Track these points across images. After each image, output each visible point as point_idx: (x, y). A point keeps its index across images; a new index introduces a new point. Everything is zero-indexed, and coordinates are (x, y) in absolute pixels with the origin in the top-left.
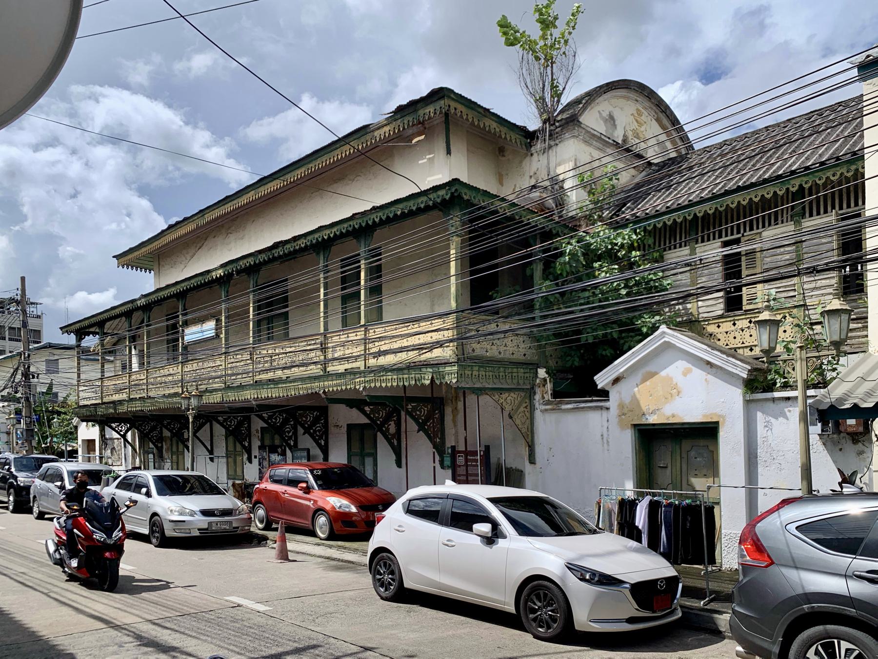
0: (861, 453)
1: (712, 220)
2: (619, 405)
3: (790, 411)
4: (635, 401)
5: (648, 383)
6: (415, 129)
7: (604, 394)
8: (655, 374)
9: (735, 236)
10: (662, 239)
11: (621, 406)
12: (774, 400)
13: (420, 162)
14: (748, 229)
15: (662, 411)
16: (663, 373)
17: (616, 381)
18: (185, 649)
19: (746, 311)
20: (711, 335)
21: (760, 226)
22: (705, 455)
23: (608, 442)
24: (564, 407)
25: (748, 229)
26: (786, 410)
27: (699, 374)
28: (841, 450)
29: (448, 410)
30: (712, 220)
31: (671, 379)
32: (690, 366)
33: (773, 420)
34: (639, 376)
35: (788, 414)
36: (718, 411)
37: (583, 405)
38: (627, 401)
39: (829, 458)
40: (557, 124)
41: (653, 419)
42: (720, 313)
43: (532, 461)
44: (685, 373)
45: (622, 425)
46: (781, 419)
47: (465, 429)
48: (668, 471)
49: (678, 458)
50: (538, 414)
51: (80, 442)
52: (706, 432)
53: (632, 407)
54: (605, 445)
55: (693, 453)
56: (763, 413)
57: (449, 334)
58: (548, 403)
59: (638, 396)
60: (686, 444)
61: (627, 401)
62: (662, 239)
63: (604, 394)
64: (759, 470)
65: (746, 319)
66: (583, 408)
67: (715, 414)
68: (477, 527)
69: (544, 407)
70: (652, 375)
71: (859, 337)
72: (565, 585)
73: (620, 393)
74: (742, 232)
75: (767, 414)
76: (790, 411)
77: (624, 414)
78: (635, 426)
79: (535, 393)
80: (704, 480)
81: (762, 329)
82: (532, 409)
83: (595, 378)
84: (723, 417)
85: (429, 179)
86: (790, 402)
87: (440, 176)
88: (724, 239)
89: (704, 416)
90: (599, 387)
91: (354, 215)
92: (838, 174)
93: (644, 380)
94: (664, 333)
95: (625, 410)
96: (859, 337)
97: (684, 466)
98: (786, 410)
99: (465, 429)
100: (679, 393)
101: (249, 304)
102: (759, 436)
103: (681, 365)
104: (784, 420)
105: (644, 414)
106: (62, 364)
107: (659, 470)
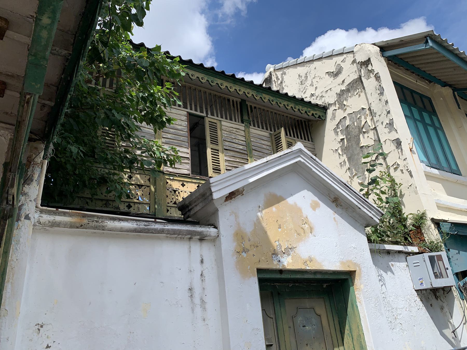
3: (392, 265)
5: (274, 209)
11: (239, 236)
15: (295, 250)
16: (291, 200)
18: (426, 68)
20: (175, 191)
23: (203, 301)
24: (110, 224)
26: (390, 263)
38: (248, 229)
41: (288, 263)
42: (186, 172)
51: (449, 272)
53: (253, 241)
54: (198, 309)
55: (299, 320)
61: (248, 229)
65: (195, 183)
67: (355, 264)
73: (237, 217)
77: (245, 250)
78: (260, 271)
95: (247, 245)
98: (390, 263)
99: (180, 169)
104: (392, 275)
105: (275, 254)
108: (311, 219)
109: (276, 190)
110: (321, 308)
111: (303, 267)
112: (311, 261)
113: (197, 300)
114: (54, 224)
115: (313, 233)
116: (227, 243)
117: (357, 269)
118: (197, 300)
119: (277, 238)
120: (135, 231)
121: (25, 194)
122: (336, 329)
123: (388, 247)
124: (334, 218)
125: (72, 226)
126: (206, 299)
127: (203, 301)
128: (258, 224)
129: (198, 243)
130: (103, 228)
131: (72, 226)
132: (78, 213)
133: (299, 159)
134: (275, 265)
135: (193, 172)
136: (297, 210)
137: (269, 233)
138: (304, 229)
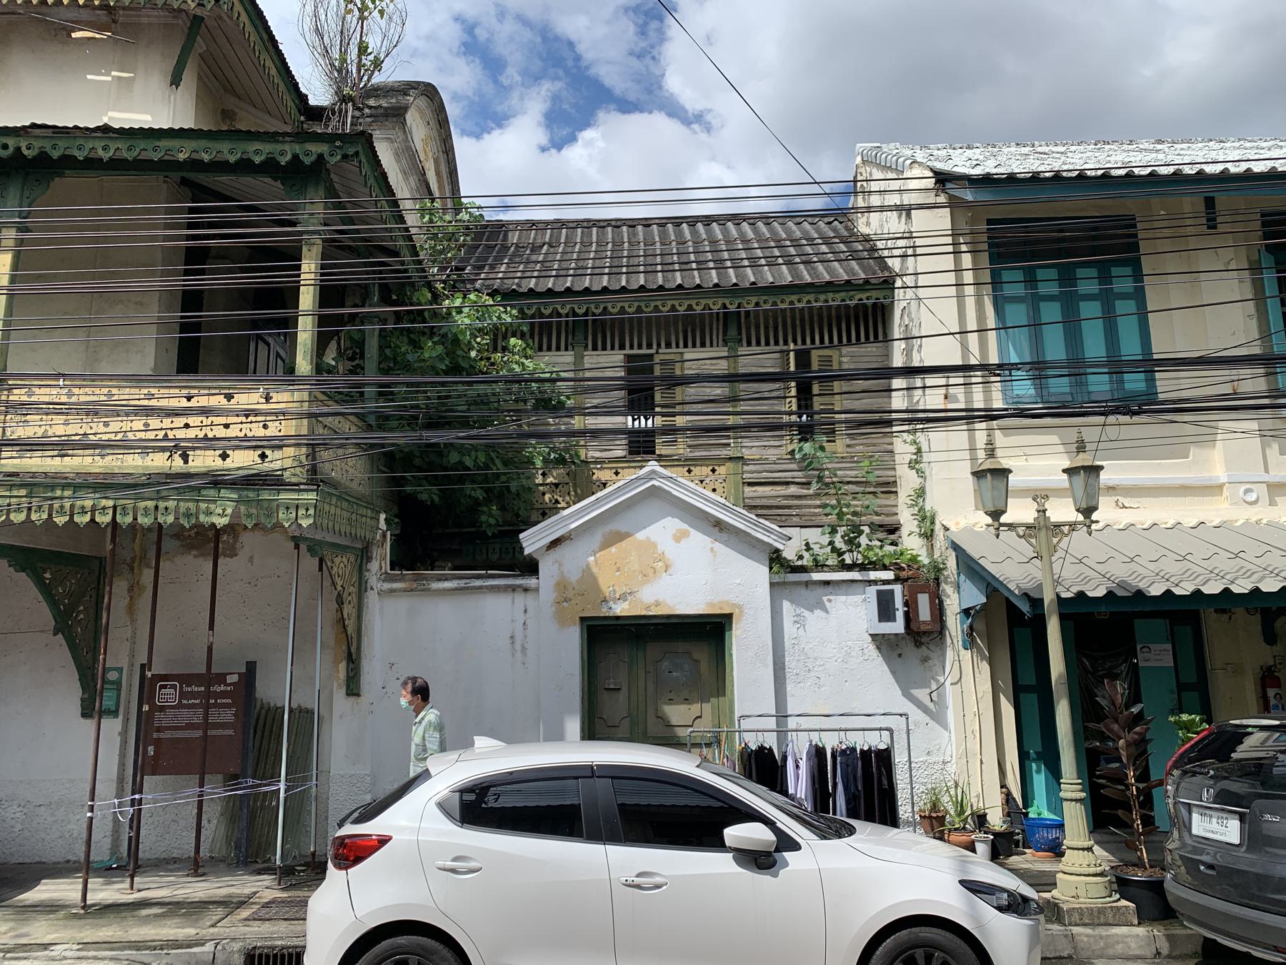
0: (925, 660)
1: (707, 322)
2: (558, 584)
4: (589, 578)
5: (613, 549)
6: (85, 15)
7: (531, 567)
8: (627, 535)
9: (644, 351)
10: (808, 332)
11: (562, 586)
12: (808, 584)
13: (89, 77)
14: (663, 345)
15: (638, 595)
16: (641, 535)
17: (555, 543)
19: (660, 456)
21: (681, 344)
22: (686, 667)
23: (523, 648)
25: (663, 345)
26: (825, 599)
27: (699, 541)
28: (900, 655)
29: (120, 587)
30: (707, 322)
31: (654, 545)
32: (685, 526)
33: (806, 613)
34: (597, 538)
35: (827, 604)
36: (732, 598)
37: (478, 583)
39: (886, 667)
40: (367, 111)
41: (621, 609)
42: (620, 453)
43: (353, 688)
44: (679, 537)
45: (561, 619)
46: (818, 612)
47: (211, 627)
48: (622, 696)
49: (642, 673)
50: (372, 599)
52: (710, 631)
54: (519, 654)
55: (665, 664)
56: (792, 602)
57: (288, 428)
58: (388, 578)
59: (595, 570)
60: (654, 650)
62: (808, 332)
63: (531, 567)
64: (789, 689)
65: (683, 466)
66: (481, 587)
67: (727, 603)
68: (733, 833)
69: (387, 586)
70: (620, 537)
71: (810, 507)
72: (980, 926)
73: (560, 565)
74: (655, 346)
75: (798, 604)
76: (830, 601)
78: (582, 619)
79: (369, 559)
80: (683, 708)
81: (995, 482)
82: (362, 587)
83: (521, 536)
84: (740, 607)
85: (110, 114)
86: (830, 589)
87: (148, 118)
88: (628, 351)
89: (710, 605)
90: (526, 552)
91: (34, 126)
92: (805, 300)
93: (606, 544)
94: (654, 472)
95: (570, 594)
96: (810, 507)
97: (651, 686)
98: (825, 599)
99: (211, 627)
100: (667, 568)
101: (292, 255)
102: (786, 637)
103: (671, 524)
105: (605, 601)
106: (1041, 274)
107: (606, 695)
108: (668, 555)
109: (618, 525)
110: (702, 653)
113: (518, 646)
114: (392, 591)
115: (670, 571)
117: (736, 612)
118: (518, 646)
119: (607, 582)
120: (456, 589)
121: (368, 570)
124: (712, 549)
125: (405, 590)
126: (527, 646)
127: (523, 648)
129: (523, 594)
130: (429, 590)
131: (405, 590)
132: (315, 638)
133: (654, 482)
134: (604, 612)
135: (631, 453)
138: (657, 565)
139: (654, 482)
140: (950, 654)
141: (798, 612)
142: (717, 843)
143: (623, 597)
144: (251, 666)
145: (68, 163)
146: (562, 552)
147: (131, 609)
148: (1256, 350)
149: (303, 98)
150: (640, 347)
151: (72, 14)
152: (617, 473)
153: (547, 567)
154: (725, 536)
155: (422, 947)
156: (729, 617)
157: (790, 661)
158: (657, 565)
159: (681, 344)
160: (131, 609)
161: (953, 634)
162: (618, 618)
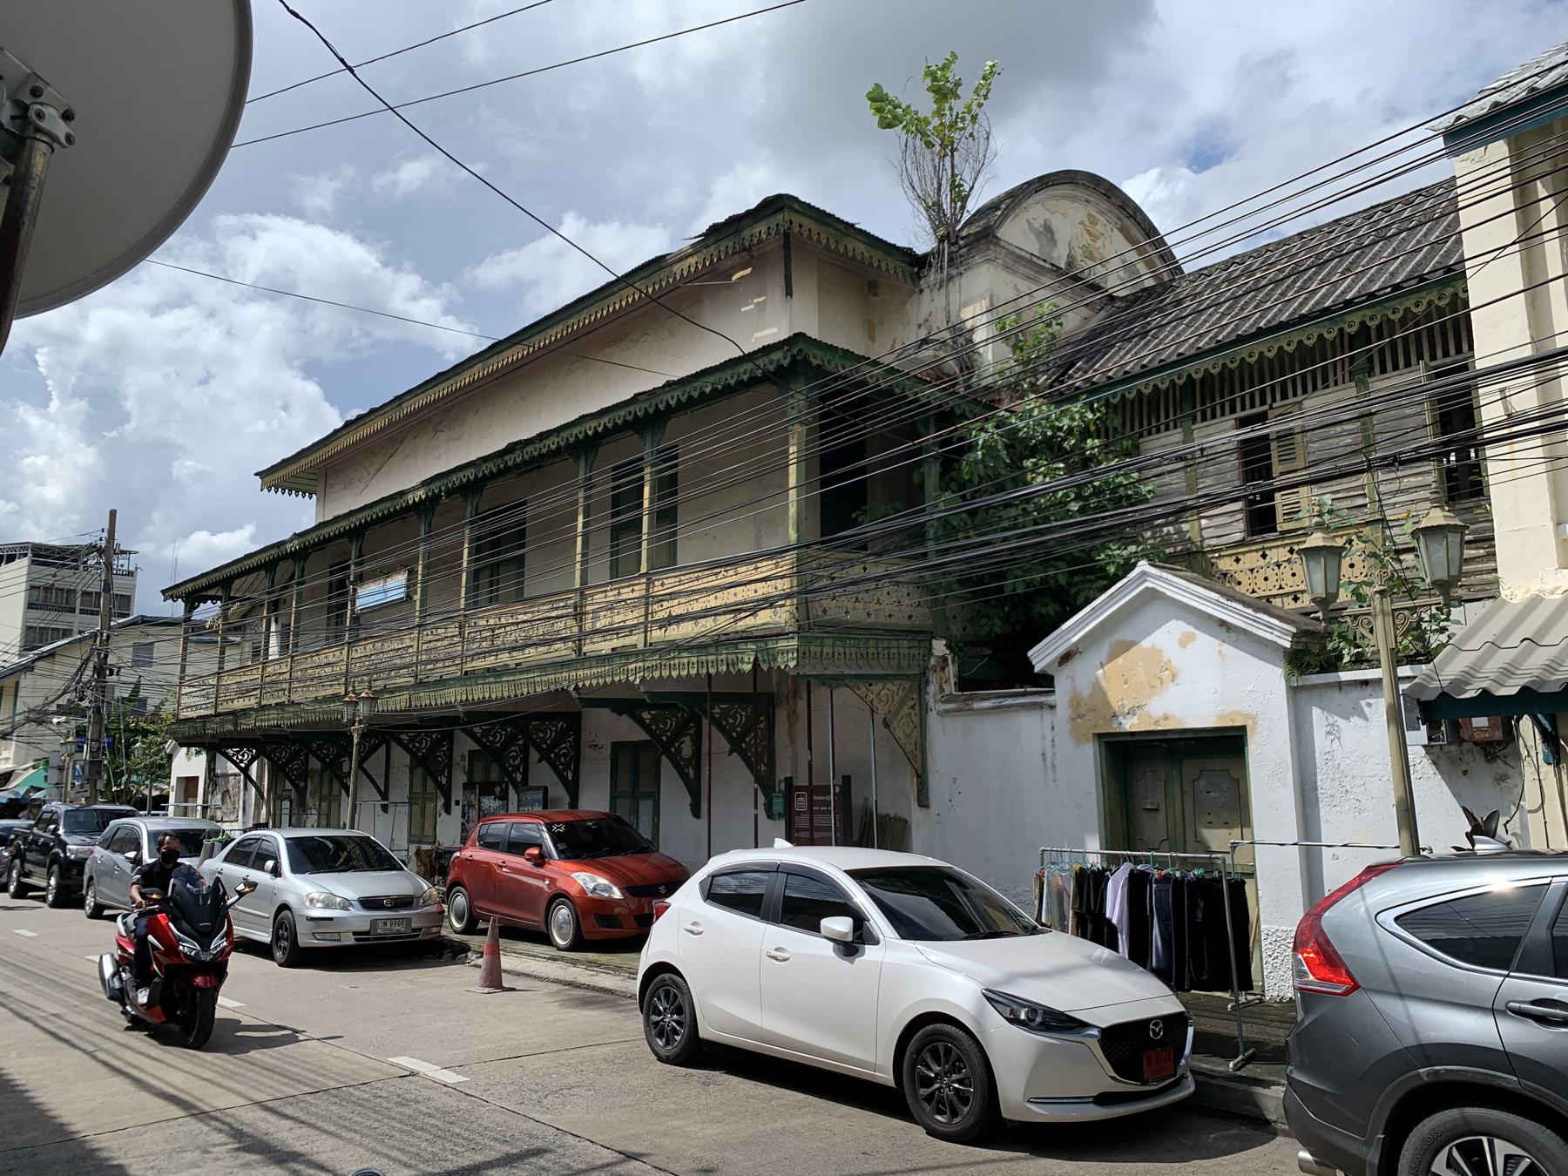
0: (1501, 778)
1: (1217, 385)
2: (1072, 700)
3: (1369, 705)
4: (1099, 692)
5: (1120, 660)
6: (737, 259)
7: (1045, 681)
9: (1258, 409)
10: (1137, 419)
11: (1075, 702)
12: (1340, 685)
14: (1278, 397)
16: (1146, 643)
17: (1066, 658)
19: (1283, 533)
21: (1299, 391)
23: (1054, 765)
25: (1278, 397)
26: (1363, 703)
27: (1206, 643)
28: (1465, 773)
29: (781, 715)
30: (1217, 385)
31: (1160, 652)
32: (1191, 629)
33: (1341, 722)
34: (1105, 650)
35: (1366, 709)
37: (1009, 701)
38: (1085, 692)
41: (1130, 724)
42: (1238, 537)
43: (923, 803)
44: (1185, 641)
45: (1077, 737)
46: (1355, 720)
48: (1161, 816)
49: (1177, 792)
50: (933, 718)
52: (1226, 745)
54: (1049, 772)
55: (1202, 784)
58: (950, 699)
59: (1104, 684)
60: (1190, 768)
61: (1085, 692)
63: (1045, 681)
64: (1322, 813)
65: (1284, 546)
66: (1010, 706)
67: (1239, 713)
70: (1127, 646)
71: (1481, 572)
72: (978, 1023)
73: (1073, 680)
75: (1330, 711)
76: (1369, 705)
78: (1100, 736)
79: (927, 683)
82: (923, 710)
84: (1254, 718)
86: (1369, 689)
87: (775, 330)
88: (1240, 414)
89: (1221, 716)
90: (1036, 670)
91: (637, 395)
92: (1425, 302)
93: (1113, 656)
94: (1144, 573)
96: (1481, 572)
98: (1363, 703)
99: (810, 748)
100: (1174, 677)
102: (1317, 751)
104: (1361, 722)
105: (1115, 716)
107: (1145, 815)
109: (1124, 634)
111: (1152, 728)
112: (1166, 718)
114: (947, 711)
116: (1063, 711)
119: (1117, 697)
122: (1286, 796)
123: (1345, 676)
128: (1097, 686)
134: (1114, 728)
136: (1156, 652)
137: (1109, 694)
138: (1165, 674)
139: (1147, 584)
140: (1529, 771)
141: (1331, 720)
142: (815, 928)
143: (1131, 712)
144: (847, 780)
145: (669, 412)
146: (1076, 667)
147: (791, 735)
148: (1527, 352)
149: (907, 253)
150: (1253, 406)
151: (729, 263)
152: (1237, 561)
153: (1061, 683)
154: (1233, 635)
155: (923, 1038)
156: (1243, 728)
157: (1324, 781)
158: (1165, 674)
159: (1299, 391)
160: (791, 735)
161: (1530, 743)
162: (1133, 734)
